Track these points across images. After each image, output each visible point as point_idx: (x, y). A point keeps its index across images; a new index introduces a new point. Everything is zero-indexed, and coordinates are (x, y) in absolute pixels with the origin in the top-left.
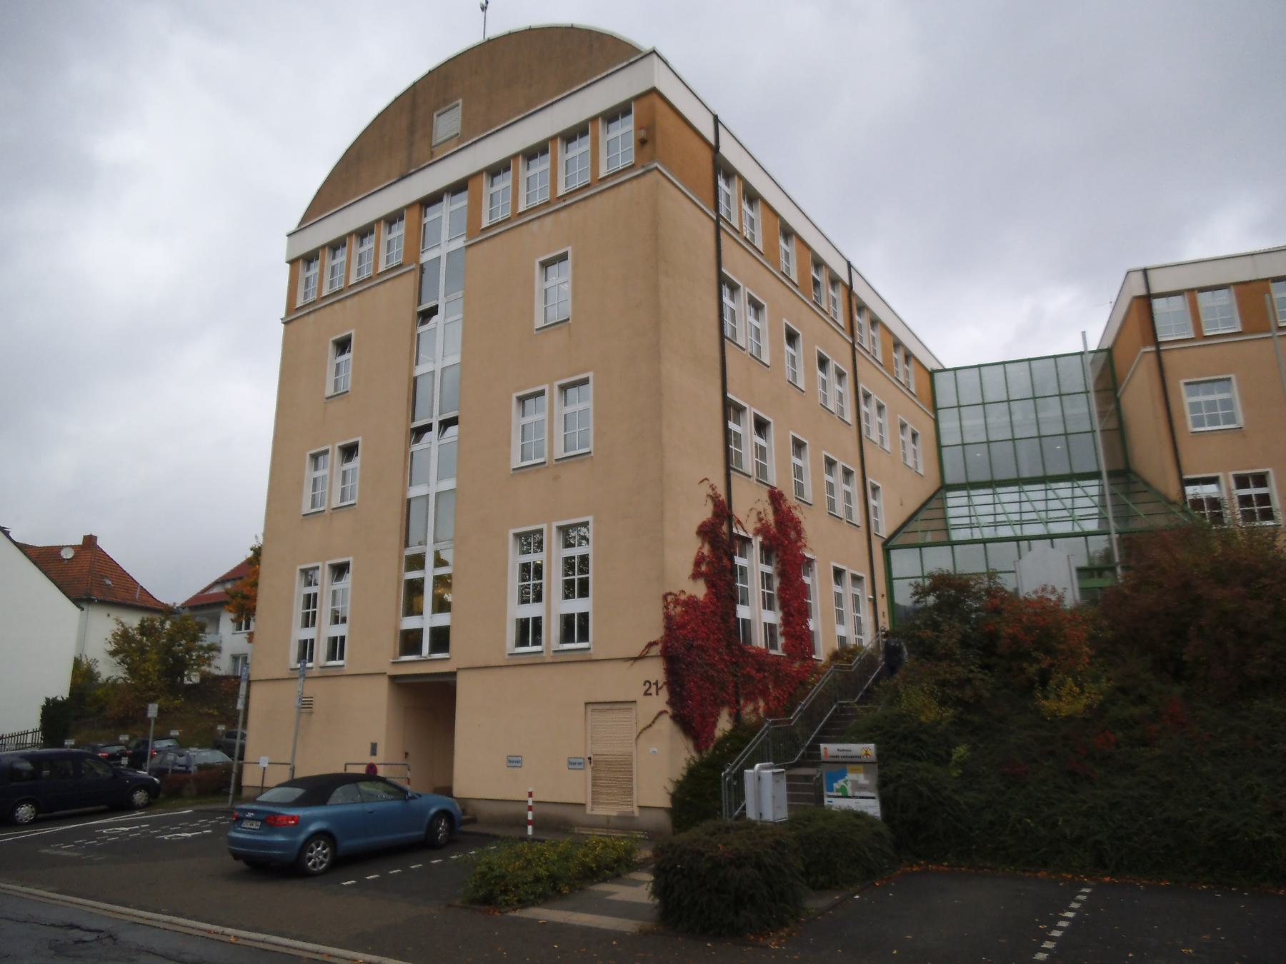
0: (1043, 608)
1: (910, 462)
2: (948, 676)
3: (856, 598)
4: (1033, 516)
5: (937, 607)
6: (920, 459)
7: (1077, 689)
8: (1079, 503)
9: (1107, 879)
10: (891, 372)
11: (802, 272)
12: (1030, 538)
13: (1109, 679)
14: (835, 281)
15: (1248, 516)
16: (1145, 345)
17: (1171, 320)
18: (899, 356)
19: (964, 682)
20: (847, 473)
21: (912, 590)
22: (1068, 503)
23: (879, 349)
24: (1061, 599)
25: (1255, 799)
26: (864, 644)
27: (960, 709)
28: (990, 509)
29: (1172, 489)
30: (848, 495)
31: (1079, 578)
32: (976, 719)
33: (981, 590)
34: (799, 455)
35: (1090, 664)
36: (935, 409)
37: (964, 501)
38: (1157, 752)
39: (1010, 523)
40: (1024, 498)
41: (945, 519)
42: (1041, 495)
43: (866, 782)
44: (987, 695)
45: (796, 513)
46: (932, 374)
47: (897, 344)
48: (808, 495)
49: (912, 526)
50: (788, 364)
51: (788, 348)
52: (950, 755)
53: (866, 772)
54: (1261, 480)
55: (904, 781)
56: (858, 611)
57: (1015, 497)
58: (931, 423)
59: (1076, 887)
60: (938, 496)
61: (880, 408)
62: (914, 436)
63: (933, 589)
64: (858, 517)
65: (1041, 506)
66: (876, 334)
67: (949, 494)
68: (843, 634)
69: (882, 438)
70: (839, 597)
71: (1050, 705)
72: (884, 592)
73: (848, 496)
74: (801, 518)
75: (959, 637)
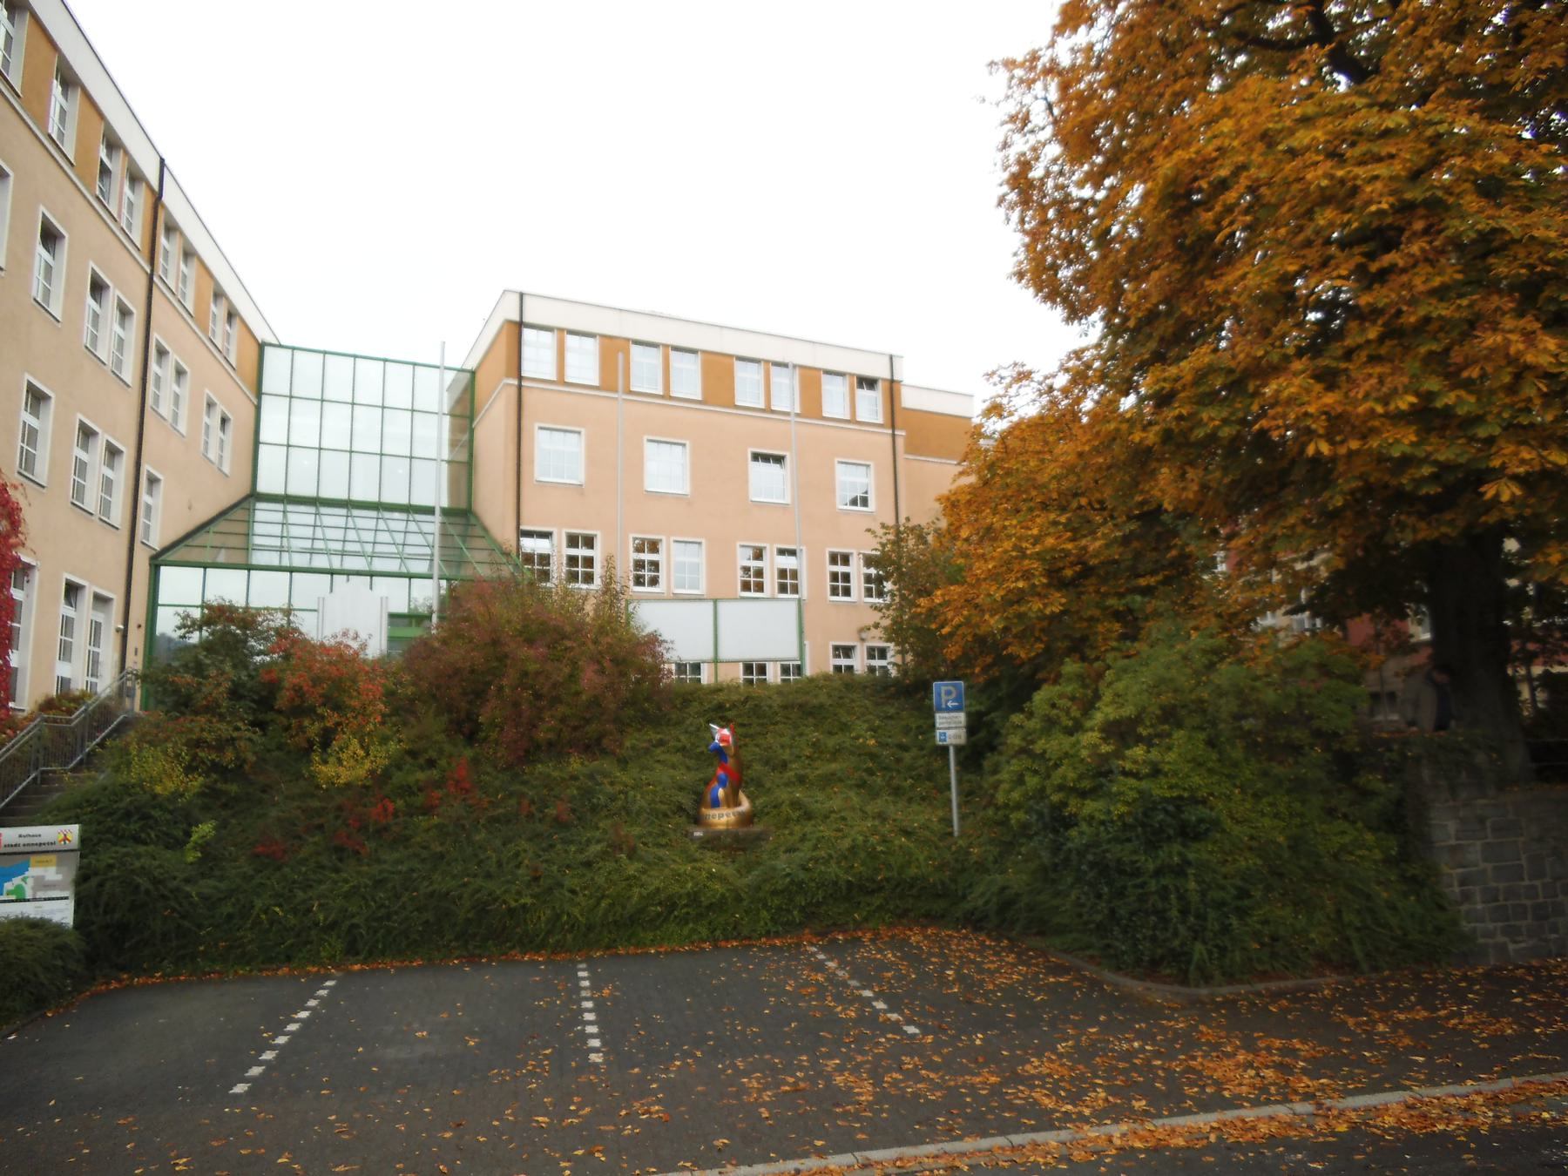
0: (341, 656)
1: (213, 455)
2: (205, 734)
3: (96, 628)
4: (356, 547)
5: (207, 646)
6: (225, 451)
7: (362, 753)
8: (412, 539)
9: (357, 967)
10: (205, 331)
11: (83, 146)
12: (349, 573)
13: (400, 741)
14: (135, 177)
15: (573, 577)
16: (508, 376)
17: (538, 356)
18: (219, 311)
19: (221, 745)
20: (113, 452)
21: (178, 621)
22: (399, 538)
23: (233, 348)
24: (364, 646)
25: (518, 866)
26: (99, 689)
27: (214, 776)
28: (308, 532)
29: (504, 532)
30: (108, 485)
31: (391, 624)
32: (233, 788)
33: (270, 629)
34: (35, 412)
35: (383, 723)
36: (259, 393)
37: (279, 517)
38: (436, 820)
39: (328, 552)
40: (351, 525)
41: (248, 535)
42: (371, 524)
43: (59, 877)
44: (252, 758)
45: (15, 495)
46: (262, 346)
47: (219, 294)
48: (42, 471)
49: (200, 539)
50: (88, 325)
51: (90, 301)
52: (188, 834)
53: (59, 864)
54: (589, 542)
55: (115, 872)
56: (96, 643)
57: (341, 522)
58: (252, 410)
59: (320, 980)
60: (245, 505)
61: (180, 373)
62: (224, 421)
63: (206, 622)
64: (119, 515)
65: (369, 536)
66: (191, 271)
67: (259, 505)
68: (67, 675)
69: (176, 415)
70: (68, 623)
71: (328, 770)
72: (143, 622)
73: (108, 485)
74: (23, 504)
75: (228, 685)
